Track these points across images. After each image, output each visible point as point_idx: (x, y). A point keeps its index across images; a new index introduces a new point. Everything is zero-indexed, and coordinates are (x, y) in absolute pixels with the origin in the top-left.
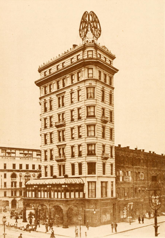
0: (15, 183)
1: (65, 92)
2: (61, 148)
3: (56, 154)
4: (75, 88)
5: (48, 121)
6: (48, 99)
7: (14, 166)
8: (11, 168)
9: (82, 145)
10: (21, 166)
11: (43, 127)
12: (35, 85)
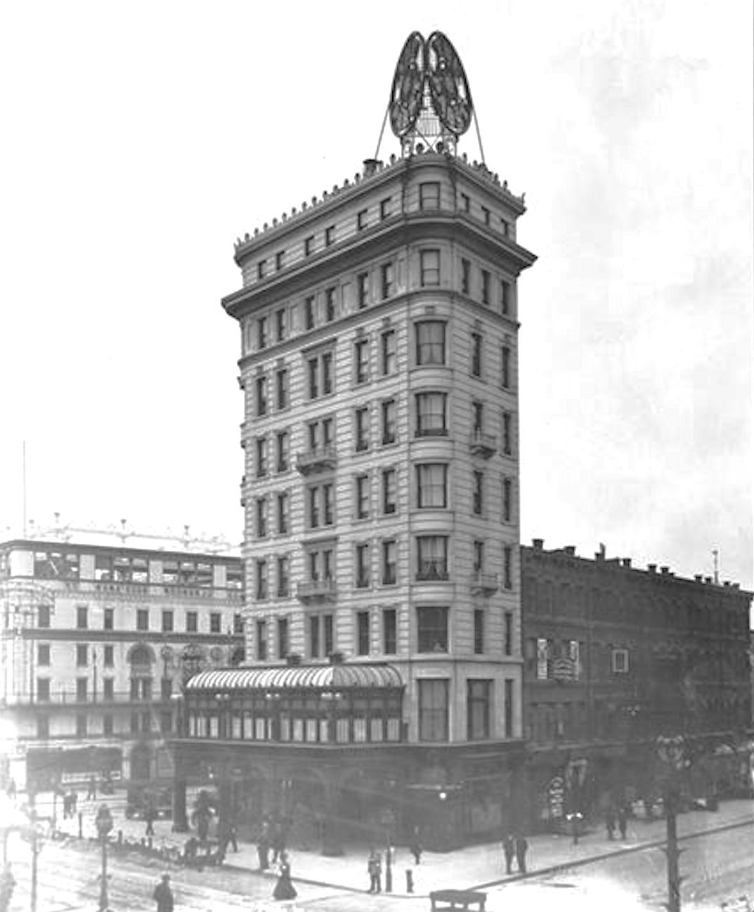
1: (335, 340)
2: (319, 554)
3: (298, 572)
4: (373, 326)
5: (271, 451)
6: (270, 364)
12: (223, 311)
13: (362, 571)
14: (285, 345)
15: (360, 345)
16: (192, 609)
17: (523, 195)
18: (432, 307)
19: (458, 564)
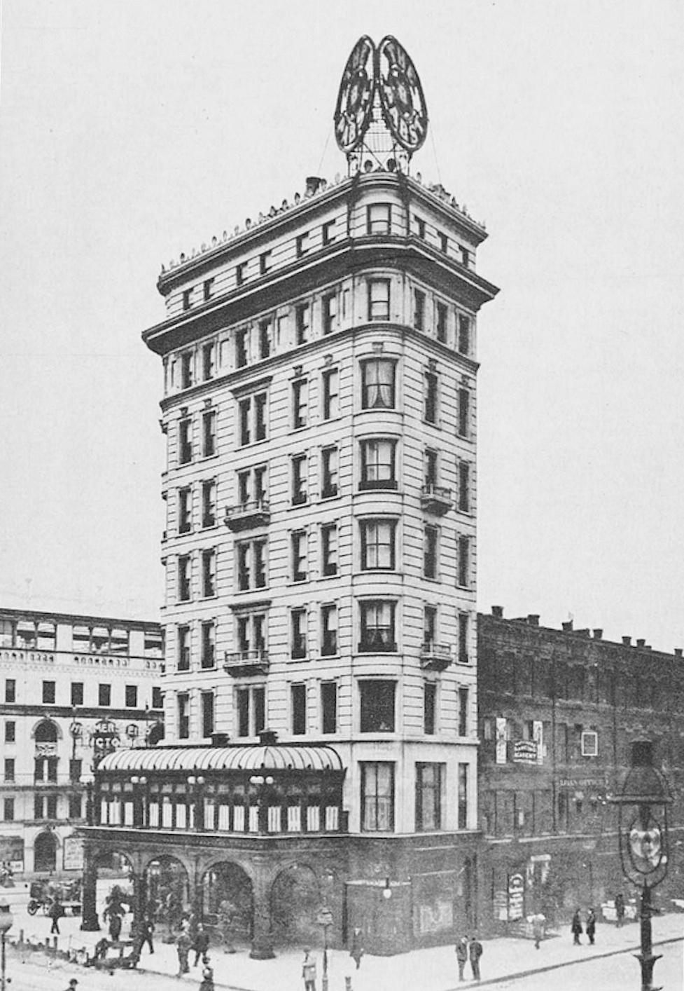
0: (54, 761)
2: (250, 618)
3: (226, 640)
4: (313, 363)
6: (195, 406)
7: (49, 688)
8: (38, 701)
10: (77, 689)
11: (176, 525)
13: (298, 639)
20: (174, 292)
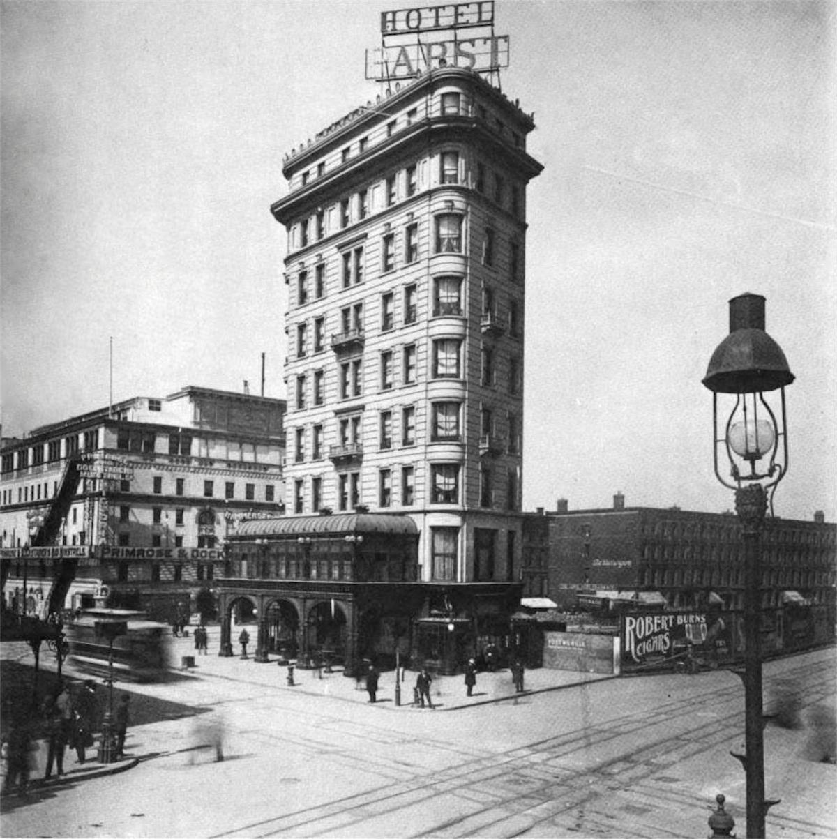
1: (365, 236)
2: (350, 418)
3: (331, 437)
4: (399, 222)
5: (310, 335)
6: (311, 260)
9: (416, 405)
11: (295, 352)
12: (272, 217)
13: (387, 317)
14: (323, 242)
15: (388, 239)
16: (251, 481)
17: (533, 114)
18: (451, 201)
19: (474, 282)
20: (295, 176)
